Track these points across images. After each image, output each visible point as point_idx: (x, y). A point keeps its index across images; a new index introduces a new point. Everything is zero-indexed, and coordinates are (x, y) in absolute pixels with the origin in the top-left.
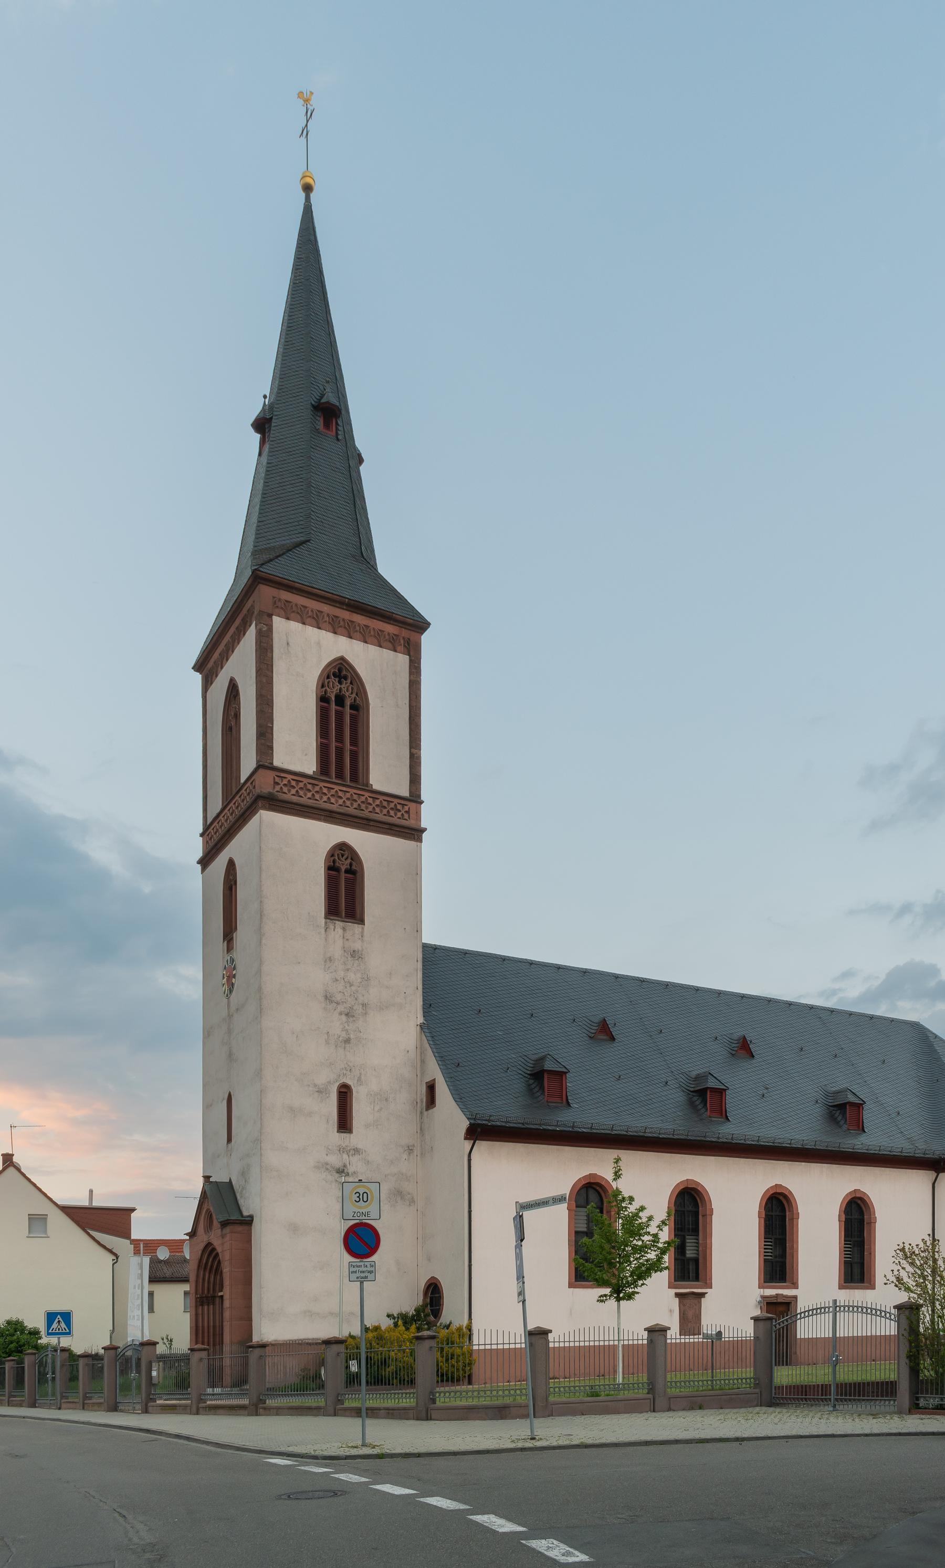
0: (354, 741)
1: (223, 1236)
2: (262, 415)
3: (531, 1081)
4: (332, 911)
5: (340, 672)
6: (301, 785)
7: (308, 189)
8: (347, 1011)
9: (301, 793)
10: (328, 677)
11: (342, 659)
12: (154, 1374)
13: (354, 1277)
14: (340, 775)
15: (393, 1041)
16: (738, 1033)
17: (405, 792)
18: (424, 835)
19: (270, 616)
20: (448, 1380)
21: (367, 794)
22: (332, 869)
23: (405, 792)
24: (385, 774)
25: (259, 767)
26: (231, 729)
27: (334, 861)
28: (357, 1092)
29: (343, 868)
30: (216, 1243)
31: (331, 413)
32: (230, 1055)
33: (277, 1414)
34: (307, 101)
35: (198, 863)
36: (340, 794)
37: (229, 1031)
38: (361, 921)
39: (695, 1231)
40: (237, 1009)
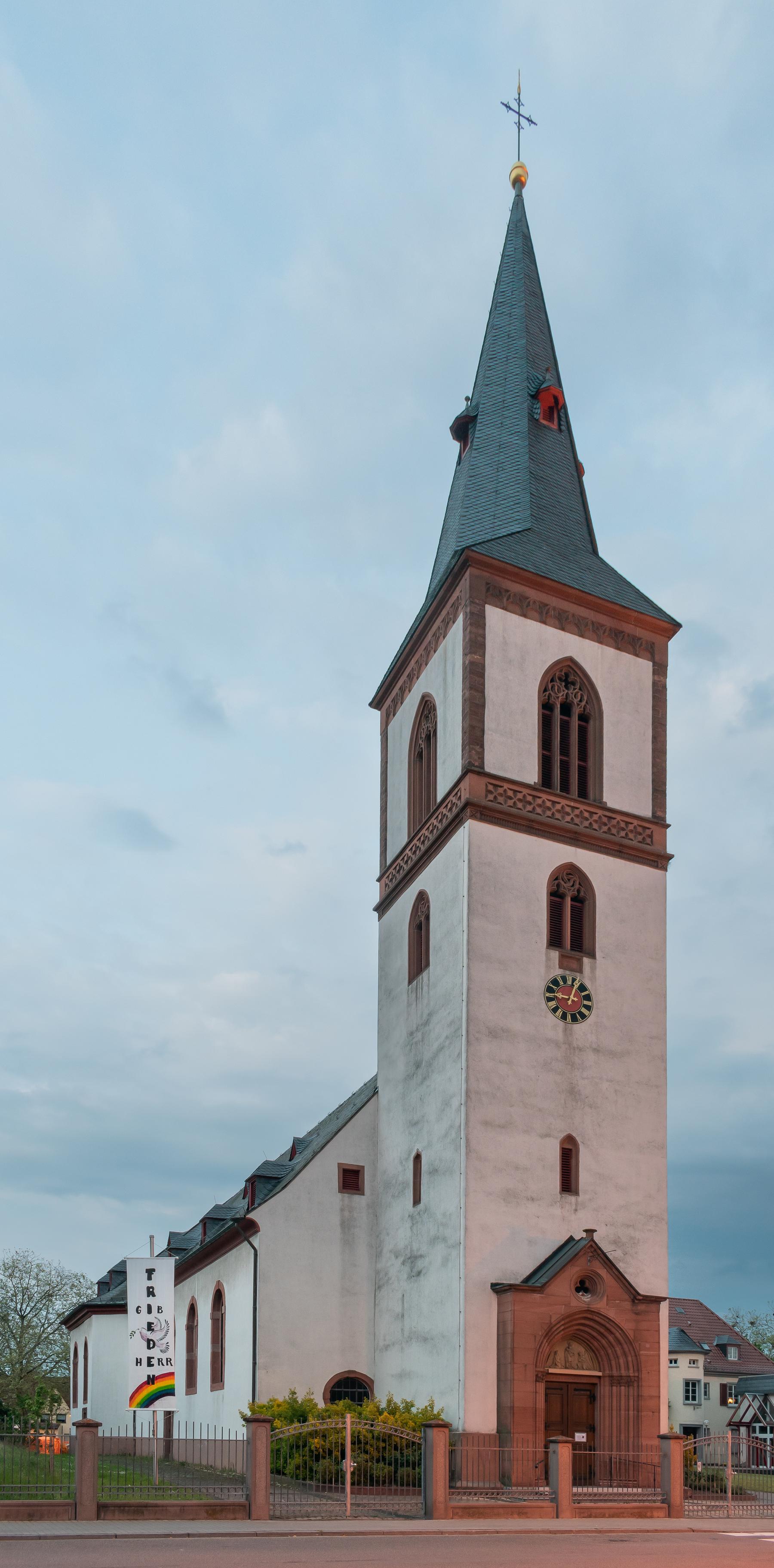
2: (465, 413)
7: (518, 183)
10: (552, 681)
11: (571, 659)
14: (565, 787)
17: (646, 811)
22: (556, 896)
23: (646, 811)
24: (621, 788)
25: (467, 771)
26: (420, 755)
27: (558, 885)
31: (548, 407)
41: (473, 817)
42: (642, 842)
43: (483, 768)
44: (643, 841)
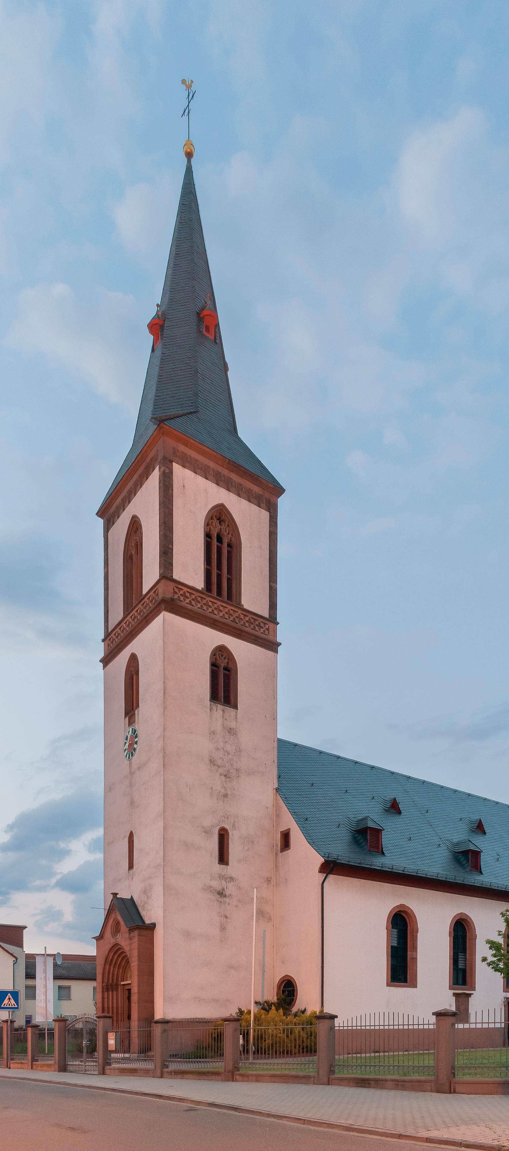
0: (229, 572)
3: (357, 835)
4: (214, 697)
5: (219, 516)
6: (193, 597)
7: (189, 155)
8: (225, 773)
9: (193, 603)
10: (212, 518)
11: (222, 505)
12: (241, 1041)
14: (219, 593)
15: (257, 800)
16: (475, 817)
17: (265, 613)
18: (279, 648)
19: (171, 462)
20: (307, 1052)
21: (240, 612)
22: (214, 665)
23: (265, 613)
24: (252, 597)
27: (216, 659)
28: (232, 835)
29: (223, 665)
32: (132, 803)
33: (257, 1081)
34: (189, 87)
35: (101, 661)
36: (221, 608)
37: (131, 785)
38: (235, 707)
39: (464, 951)
40: (139, 768)
42: (262, 632)
43: (172, 577)
44: (264, 633)
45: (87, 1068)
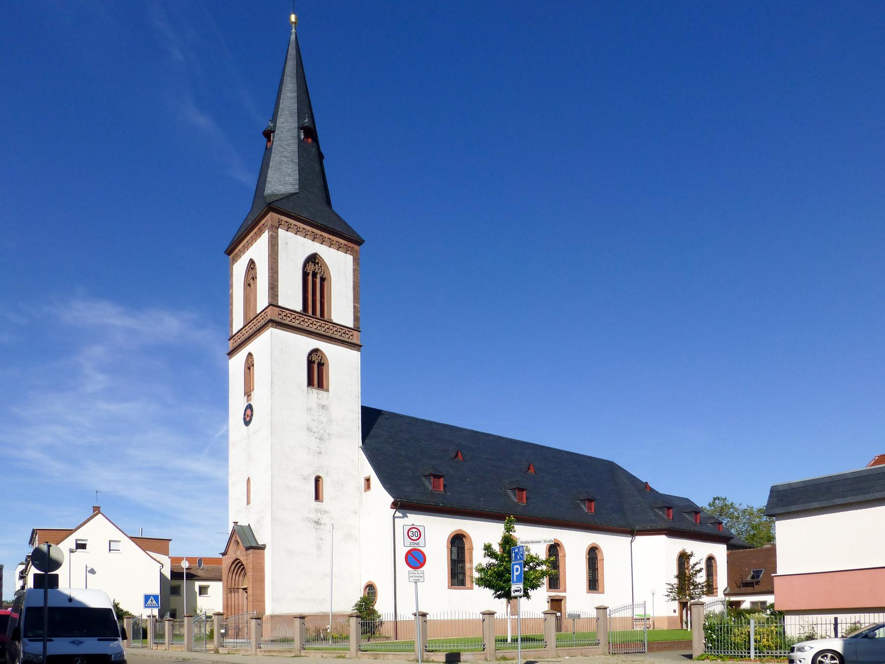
1: (247, 555)
4: (310, 383)
13: (412, 579)
22: (310, 363)
25: (270, 305)
30: (242, 559)
38: (328, 390)
41: (272, 326)
45: (793, 626)
